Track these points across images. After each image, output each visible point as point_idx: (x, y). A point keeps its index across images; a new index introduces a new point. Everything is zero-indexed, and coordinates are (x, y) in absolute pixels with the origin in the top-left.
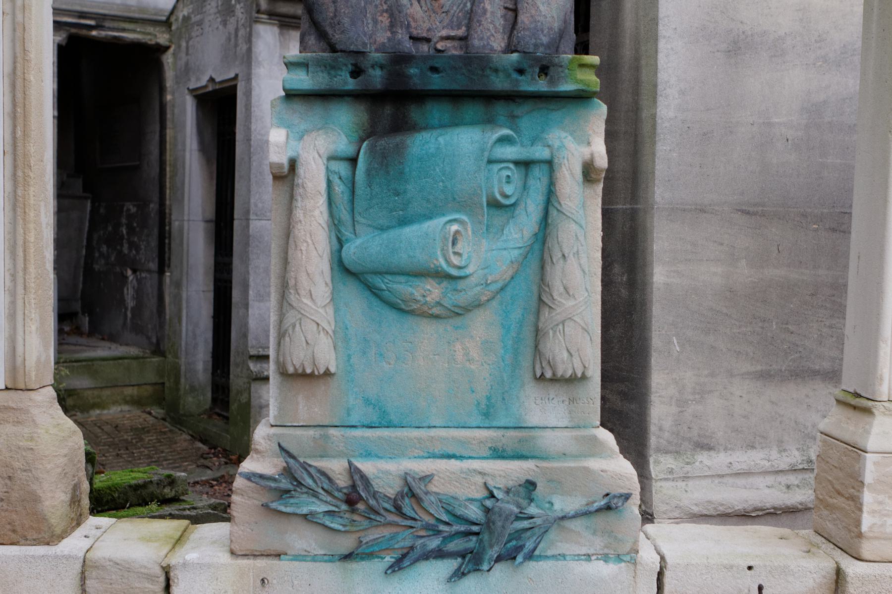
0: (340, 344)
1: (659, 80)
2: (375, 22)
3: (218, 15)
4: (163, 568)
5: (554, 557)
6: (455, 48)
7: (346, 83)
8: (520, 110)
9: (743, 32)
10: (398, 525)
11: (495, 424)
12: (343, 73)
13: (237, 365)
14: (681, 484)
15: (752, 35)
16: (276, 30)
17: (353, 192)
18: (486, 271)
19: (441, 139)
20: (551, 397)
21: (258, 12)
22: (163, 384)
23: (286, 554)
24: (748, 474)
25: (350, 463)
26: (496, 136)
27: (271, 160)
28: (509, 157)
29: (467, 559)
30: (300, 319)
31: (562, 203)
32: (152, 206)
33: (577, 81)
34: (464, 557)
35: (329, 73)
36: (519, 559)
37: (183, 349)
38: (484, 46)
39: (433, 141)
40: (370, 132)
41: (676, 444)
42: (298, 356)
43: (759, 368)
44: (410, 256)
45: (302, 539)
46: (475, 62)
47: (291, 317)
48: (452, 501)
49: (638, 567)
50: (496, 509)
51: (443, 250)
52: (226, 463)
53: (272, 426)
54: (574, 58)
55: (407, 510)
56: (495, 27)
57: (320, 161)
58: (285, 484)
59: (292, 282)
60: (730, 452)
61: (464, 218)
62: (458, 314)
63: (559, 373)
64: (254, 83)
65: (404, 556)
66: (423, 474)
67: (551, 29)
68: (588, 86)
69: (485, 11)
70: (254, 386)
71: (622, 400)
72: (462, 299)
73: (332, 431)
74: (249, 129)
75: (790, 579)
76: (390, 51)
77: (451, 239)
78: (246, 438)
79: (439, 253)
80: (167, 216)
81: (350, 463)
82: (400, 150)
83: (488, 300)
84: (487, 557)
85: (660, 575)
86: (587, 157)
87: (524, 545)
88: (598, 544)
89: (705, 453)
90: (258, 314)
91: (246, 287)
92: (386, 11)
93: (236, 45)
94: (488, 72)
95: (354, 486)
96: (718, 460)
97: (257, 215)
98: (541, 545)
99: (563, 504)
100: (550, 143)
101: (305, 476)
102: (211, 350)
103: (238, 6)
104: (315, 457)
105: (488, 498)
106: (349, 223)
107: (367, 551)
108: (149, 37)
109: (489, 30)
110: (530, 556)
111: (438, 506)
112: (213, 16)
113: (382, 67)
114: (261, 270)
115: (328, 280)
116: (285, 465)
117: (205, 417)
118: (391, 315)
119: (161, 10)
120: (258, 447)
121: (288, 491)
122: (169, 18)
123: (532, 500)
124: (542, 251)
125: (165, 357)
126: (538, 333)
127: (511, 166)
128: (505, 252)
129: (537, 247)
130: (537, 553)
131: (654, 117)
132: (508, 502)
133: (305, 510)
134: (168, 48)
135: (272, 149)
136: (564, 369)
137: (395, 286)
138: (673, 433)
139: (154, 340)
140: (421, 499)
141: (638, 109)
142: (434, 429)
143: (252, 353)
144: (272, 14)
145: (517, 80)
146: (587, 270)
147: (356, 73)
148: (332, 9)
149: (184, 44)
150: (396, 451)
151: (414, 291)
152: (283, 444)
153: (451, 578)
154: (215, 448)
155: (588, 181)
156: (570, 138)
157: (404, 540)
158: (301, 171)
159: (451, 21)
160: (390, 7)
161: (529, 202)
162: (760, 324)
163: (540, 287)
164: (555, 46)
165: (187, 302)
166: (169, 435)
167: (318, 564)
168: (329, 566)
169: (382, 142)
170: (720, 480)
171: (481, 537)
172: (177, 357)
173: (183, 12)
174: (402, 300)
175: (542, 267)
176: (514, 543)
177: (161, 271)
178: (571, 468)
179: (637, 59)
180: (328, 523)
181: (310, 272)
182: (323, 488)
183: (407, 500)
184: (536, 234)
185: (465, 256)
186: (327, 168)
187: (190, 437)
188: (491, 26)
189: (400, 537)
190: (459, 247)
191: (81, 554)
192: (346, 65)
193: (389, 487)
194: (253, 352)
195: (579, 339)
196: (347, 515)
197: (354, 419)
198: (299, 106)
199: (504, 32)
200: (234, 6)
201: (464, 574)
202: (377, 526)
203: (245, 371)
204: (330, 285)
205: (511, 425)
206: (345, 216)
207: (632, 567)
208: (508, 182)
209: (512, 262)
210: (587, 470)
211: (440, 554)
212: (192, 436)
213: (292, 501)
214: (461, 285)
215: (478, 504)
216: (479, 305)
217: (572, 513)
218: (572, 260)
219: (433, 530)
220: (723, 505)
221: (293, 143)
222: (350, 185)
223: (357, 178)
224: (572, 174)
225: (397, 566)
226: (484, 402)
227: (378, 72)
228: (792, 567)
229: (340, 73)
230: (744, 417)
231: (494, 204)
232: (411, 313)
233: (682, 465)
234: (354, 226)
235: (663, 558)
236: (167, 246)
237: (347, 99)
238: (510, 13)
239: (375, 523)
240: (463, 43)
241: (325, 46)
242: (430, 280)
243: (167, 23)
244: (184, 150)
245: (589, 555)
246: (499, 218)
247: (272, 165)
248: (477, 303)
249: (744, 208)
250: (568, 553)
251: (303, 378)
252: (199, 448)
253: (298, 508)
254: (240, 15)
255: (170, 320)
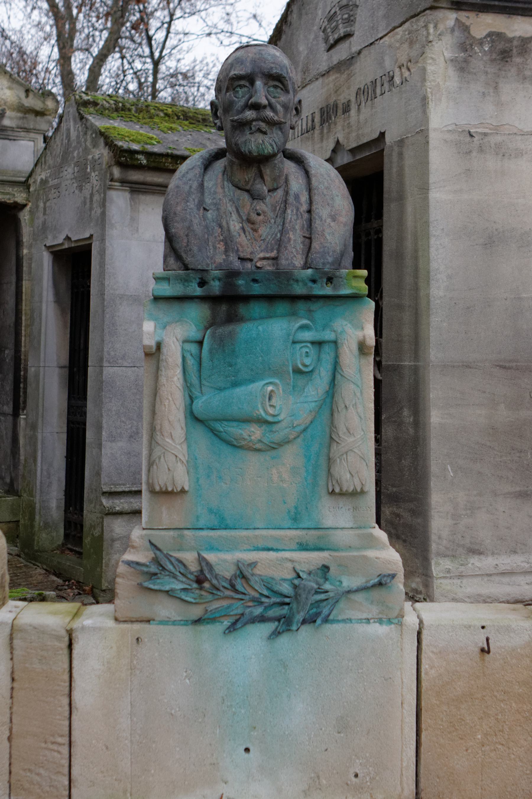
0: (191, 470)
1: (431, 268)
2: (215, 248)
3: (74, 181)
4: (67, 631)
5: (344, 621)
6: (270, 266)
7: (195, 291)
8: (314, 306)
9: (496, 230)
10: (233, 598)
11: (301, 526)
12: (193, 284)
13: (91, 502)
14: (457, 581)
15: (503, 232)
16: (127, 195)
17: (200, 364)
18: (293, 417)
19: (260, 328)
20: (340, 506)
21: (112, 180)
22: (18, 521)
23: (154, 620)
24: (511, 573)
25: (199, 554)
26: (297, 325)
27: (144, 344)
28: (308, 339)
29: (281, 622)
30: (164, 453)
31: (344, 370)
32: (7, 352)
33: (352, 288)
34: (279, 620)
35: (184, 285)
36: (319, 621)
37: (38, 487)
38: (289, 264)
39: (255, 329)
40: (212, 323)
41: (453, 549)
42: (162, 480)
43: (518, 489)
44: (239, 408)
45: (166, 609)
46: (283, 276)
47: (157, 452)
48: (270, 580)
49: (404, 627)
50: (302, 586)
51: (262, 404)
52: (79, 594)
53: (144, 529)
54: (350, 272)
55: (239, 587)
56: (297, 250)
57: (177, 344)
58: (153, 569)
59: (158, 427)
60: (496, 556)
61: (277, 381)
62: (274, 448)
63: (344, 489)
64: (107, 244)
65: (237, 621)
66: (250, 562)
67: (334, 251)
68: (360, 290)
69: (290, 239)
70: (107, 521)
71: (411, 516)
72: (277, 437)
73: (186, 532)
74: (103, 284)
75: (512, 635)
76: (225, 268)
77: (268, 396)
78: (98, 569)
79: (259, 406)
80: (23, 361)
81: (199, 554)
82: (231, 335)
83: (295, 438)
84: (296, 620)
85: (419, 633)
86: (361, 338)
87: (322, 612)
88: (374, 611)
89: (476, 557)
90: (110, 455)
91: (99, 428)
92: (222, 241)
93: (91, 209)
94: (292, 282)
95: (202, 571)
96: (487, 563)
97: (109, 362)
98: (334, 612)
99: (349, 582)
100: (335, 329)
101: (168, 563)
102: (64, 488)
103: (93, 174)
104: (174, 550)
105: (296, 578)
106: (198, 386)
107: (211, 617)
108: (8, 197)
109: (292, 252)
110: (326, 620)
111: (260, 584)
112: (69, 182)
113: (219, 280)
114: (114, 413)
115: (183, 425)
116: (153, 556)
117: (58, 552)
118: (226, 450)
119: (20, 172)
120: (135, 544)
121: (155, 574)
122: (27, 180)
123: (326, 579)
124: (332, 403)
125: (20, 496)
126: (330, 461)
127: (309, 345)
128: (306, 405)
129: (328, 400)
130: (331, 617)
131: (428, 295)
132: (310, 581)
133: (167, 588)
134: (25, 206)
135: (145, 337)
136: (348, 487)
137: (229, 429)
138: (450, 541)
139: (8, 480)
140: (249, 579)
141: (417, 289)
142: (258, 530)
143: (104, 490)
144: (123, 182)
145: (311, 287)
146: (362, 417)
147: (202, 283)
148: (186, 241)
149: (41, 205)
150: (232, 545)
151: (243, 432)
152: (153, 541)
153: (270, 636)
154: (69, 581)
155: (363, 354)
156: (349, 325)
157: (237, 608)
158: (164, 350)
159: (267, 247)
160: (225, 238)
161: (322, 369)
162: (518, 455)
163: (331, 428)
164: (338, 264)
165: (43, 443)
166: (24, 569)
167: (176, 627)
168: (184, 629)
169: (220, 330)
170: (489, 578)
171: (291, 605)
172: (32, 496)
173: (41, 175)
174: (235, 439)
175: (332, 415)
176: (314, 610)
177: (16, 414)
178: (355, 557)
179: (416, 251)
180: (183, 597)
181: (171, 420)
182: (180, 572)
183: (239, 580)
184: (327, 392)
185: (278, 408)
186: (182, 348)
187: (44, 571)
188: (294, 250)
189: (234, 607)
190: (273, 402)
191: (11, 621)
192: (195, 279)
193: (228, 572)
194: (106, 489)
195: (358, 463)
196: (197, 591)
197: (201, 524)
198: (163, 305)
199: (303, 254)
200: (89, 174)
201: (279, 633)
202: (218, 599)
203: (98, 507)
204: (185, 428)
205: (312, 527)
206: (195, 380)
207: (399, 628)
208: (307, 356)
209: (311, 411)
210: (365, 557)
211: (262, 619)
212: (46, 570)
213: (158, 581)
214: (275, 428)
215: (289, 582)
216: (287, 442)
217: (355, 588)
218: (351, 409)
219: (258, 602)
220: (490, 597)
221: (159, 331)
222: (198, 360)
223: (203, 355)
224: (351, 351)
225: (232, 628)
226: (293, 510)
227: (217, 283)
228: (513, 626)
229: (191, 284)
230: (507, 528)
231: (297, 371)
232: (240, 447)
233: (458, 566)
234: (201, 387)
235: (421, 622)
236: (22, 390)
237: (196, 300)
238: (307, 240)
239: (216, 597)
240: (275, 261)
241: (181, 265)
242: (254, 425)
243: (25, 184)
244: (41, 302)
245: (368, 619)
246: (301, 381)
247: (144, 347)
248: (287, 440)
249: (501, 364)
250: (353, 617)
251: (167, 494)
252: (54, 581)
253: (163, 586)
254: (95, 182)
255: (25, 460)
